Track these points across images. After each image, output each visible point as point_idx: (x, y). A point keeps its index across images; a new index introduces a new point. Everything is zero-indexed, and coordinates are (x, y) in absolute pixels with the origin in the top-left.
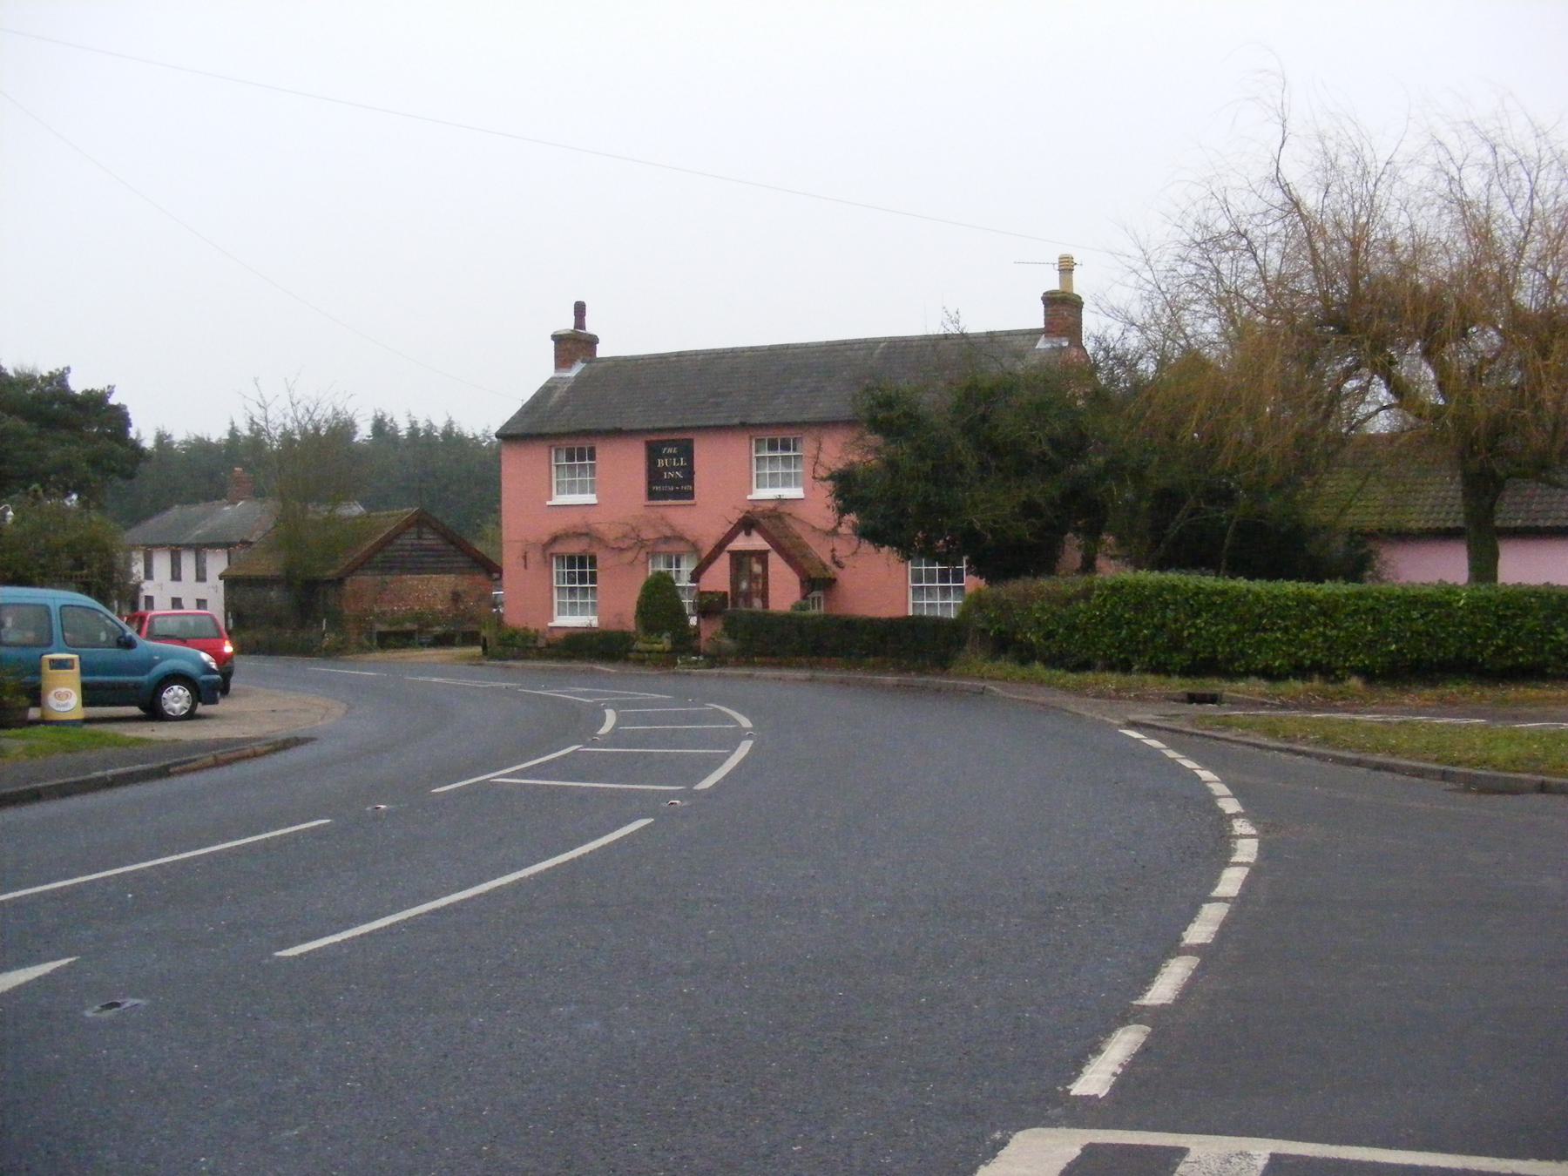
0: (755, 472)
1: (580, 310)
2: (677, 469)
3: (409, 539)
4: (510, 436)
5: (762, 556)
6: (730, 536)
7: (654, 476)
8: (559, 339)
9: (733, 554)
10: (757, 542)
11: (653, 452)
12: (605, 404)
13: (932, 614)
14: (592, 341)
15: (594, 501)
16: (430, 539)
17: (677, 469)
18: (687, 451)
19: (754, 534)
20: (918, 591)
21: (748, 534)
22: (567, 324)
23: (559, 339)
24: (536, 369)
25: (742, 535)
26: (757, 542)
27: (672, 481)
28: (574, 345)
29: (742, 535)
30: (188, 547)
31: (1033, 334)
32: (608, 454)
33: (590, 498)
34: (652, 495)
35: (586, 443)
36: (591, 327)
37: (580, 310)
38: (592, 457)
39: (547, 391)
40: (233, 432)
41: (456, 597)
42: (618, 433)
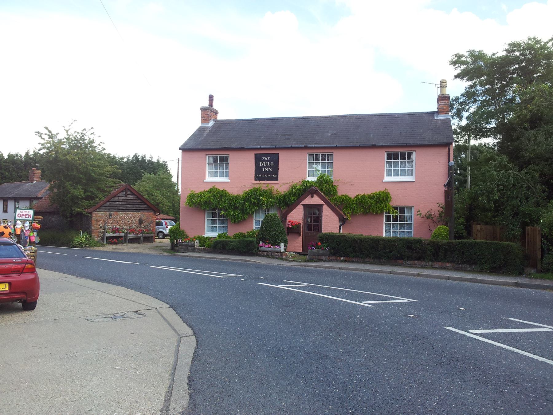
1: (211, 98)
2: (270, 167)
3: (122, 196)
5: (319, 207)
7: (258, 170)
8: (203, 109)
9: (304, 206)
10: (316, 200)
11: (258, 159)
12: (216, 139)
13: (401, 237)
14: (216, 113)
15: (229, 181)
16: (130, 197)
17: (270, 167)
18: (275, 159)
20: (388, 226)
22: (206, 104)
23: (203, 109)
24: (194, 123)
26: (316, 200)
27: (266, 173)
28: (208, 112)
30: (11, 199)
31: (432, 114)
32: (235, 159)
34: (257, 178)
36: (215, 106)
37: (211, 98)
38: (227, 161)
39: (200, 131)
40: (27, 153)
41: (141, 222)
42: (242, 149)
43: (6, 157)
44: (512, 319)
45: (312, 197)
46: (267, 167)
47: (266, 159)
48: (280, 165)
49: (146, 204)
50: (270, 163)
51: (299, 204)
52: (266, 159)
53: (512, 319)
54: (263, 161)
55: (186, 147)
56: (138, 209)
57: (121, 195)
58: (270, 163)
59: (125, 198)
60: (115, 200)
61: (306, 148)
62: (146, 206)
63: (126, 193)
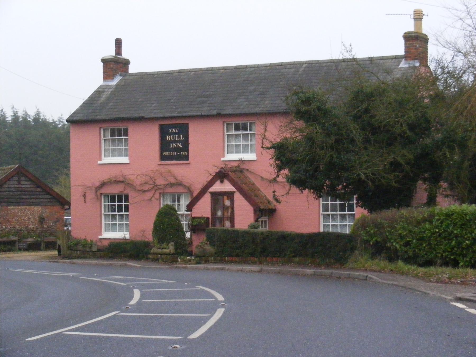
0: (226, 144)
1: (118, 43)
2: (179, 141)
3: (13, 184)
4: (73, 121)
5: (230, 195)
6: (211, 183)
8: (105, 61)
9: (210, 192)
10: (227, 187)
11: (163, 131)
13: (335, 231)
14: (126, 63)
16: (26, 184)
17: (179, 141)
18: (184, 130)
19: (226, 182)
21: (222, 182)
22: (111, 52)
23: (105, 61)
24: (92, 80)
25: (218, 183)
27: (176, 149)
28: (115, 65)
29: (218, 183)
31: (397, 58)
33: (125, 160)
34: (163, 158)
35: (122, 126)
36: (125, 55)
37: (118, 43)
38: (126, 134)
39: (98, 93)
42: (141, 120)
43: (9, 119)
44: (211, 300)
45: (222, 182)
46: (175, 142)
47: (174, 130)
48: (191, 140)
49: (49, 194)
50: (179, 137)
51: (207, 192)
52: (174, 130)
53: (211, 300)
54: (170, 134)
55: (75, 119)
56: (37, 200)
57: (12, 182)
58: (179, 137)
59: (18, 186)
60: (3, 190)
61: (219, 115)
62: (49, 197)
63: (19, 178)
